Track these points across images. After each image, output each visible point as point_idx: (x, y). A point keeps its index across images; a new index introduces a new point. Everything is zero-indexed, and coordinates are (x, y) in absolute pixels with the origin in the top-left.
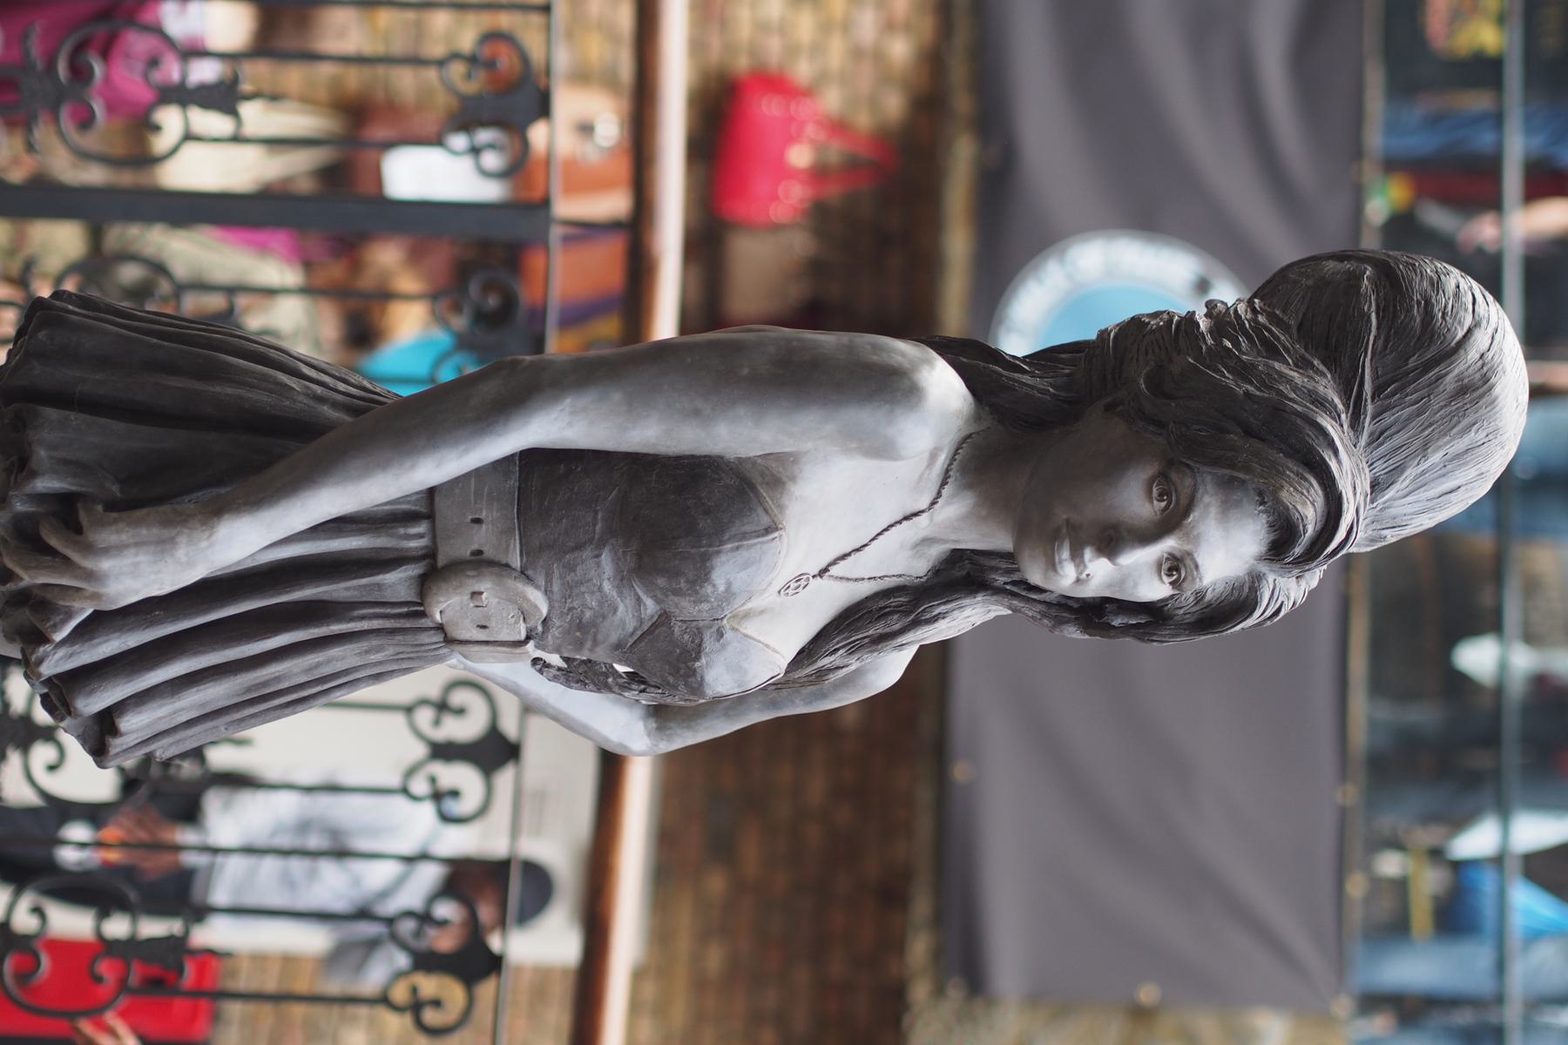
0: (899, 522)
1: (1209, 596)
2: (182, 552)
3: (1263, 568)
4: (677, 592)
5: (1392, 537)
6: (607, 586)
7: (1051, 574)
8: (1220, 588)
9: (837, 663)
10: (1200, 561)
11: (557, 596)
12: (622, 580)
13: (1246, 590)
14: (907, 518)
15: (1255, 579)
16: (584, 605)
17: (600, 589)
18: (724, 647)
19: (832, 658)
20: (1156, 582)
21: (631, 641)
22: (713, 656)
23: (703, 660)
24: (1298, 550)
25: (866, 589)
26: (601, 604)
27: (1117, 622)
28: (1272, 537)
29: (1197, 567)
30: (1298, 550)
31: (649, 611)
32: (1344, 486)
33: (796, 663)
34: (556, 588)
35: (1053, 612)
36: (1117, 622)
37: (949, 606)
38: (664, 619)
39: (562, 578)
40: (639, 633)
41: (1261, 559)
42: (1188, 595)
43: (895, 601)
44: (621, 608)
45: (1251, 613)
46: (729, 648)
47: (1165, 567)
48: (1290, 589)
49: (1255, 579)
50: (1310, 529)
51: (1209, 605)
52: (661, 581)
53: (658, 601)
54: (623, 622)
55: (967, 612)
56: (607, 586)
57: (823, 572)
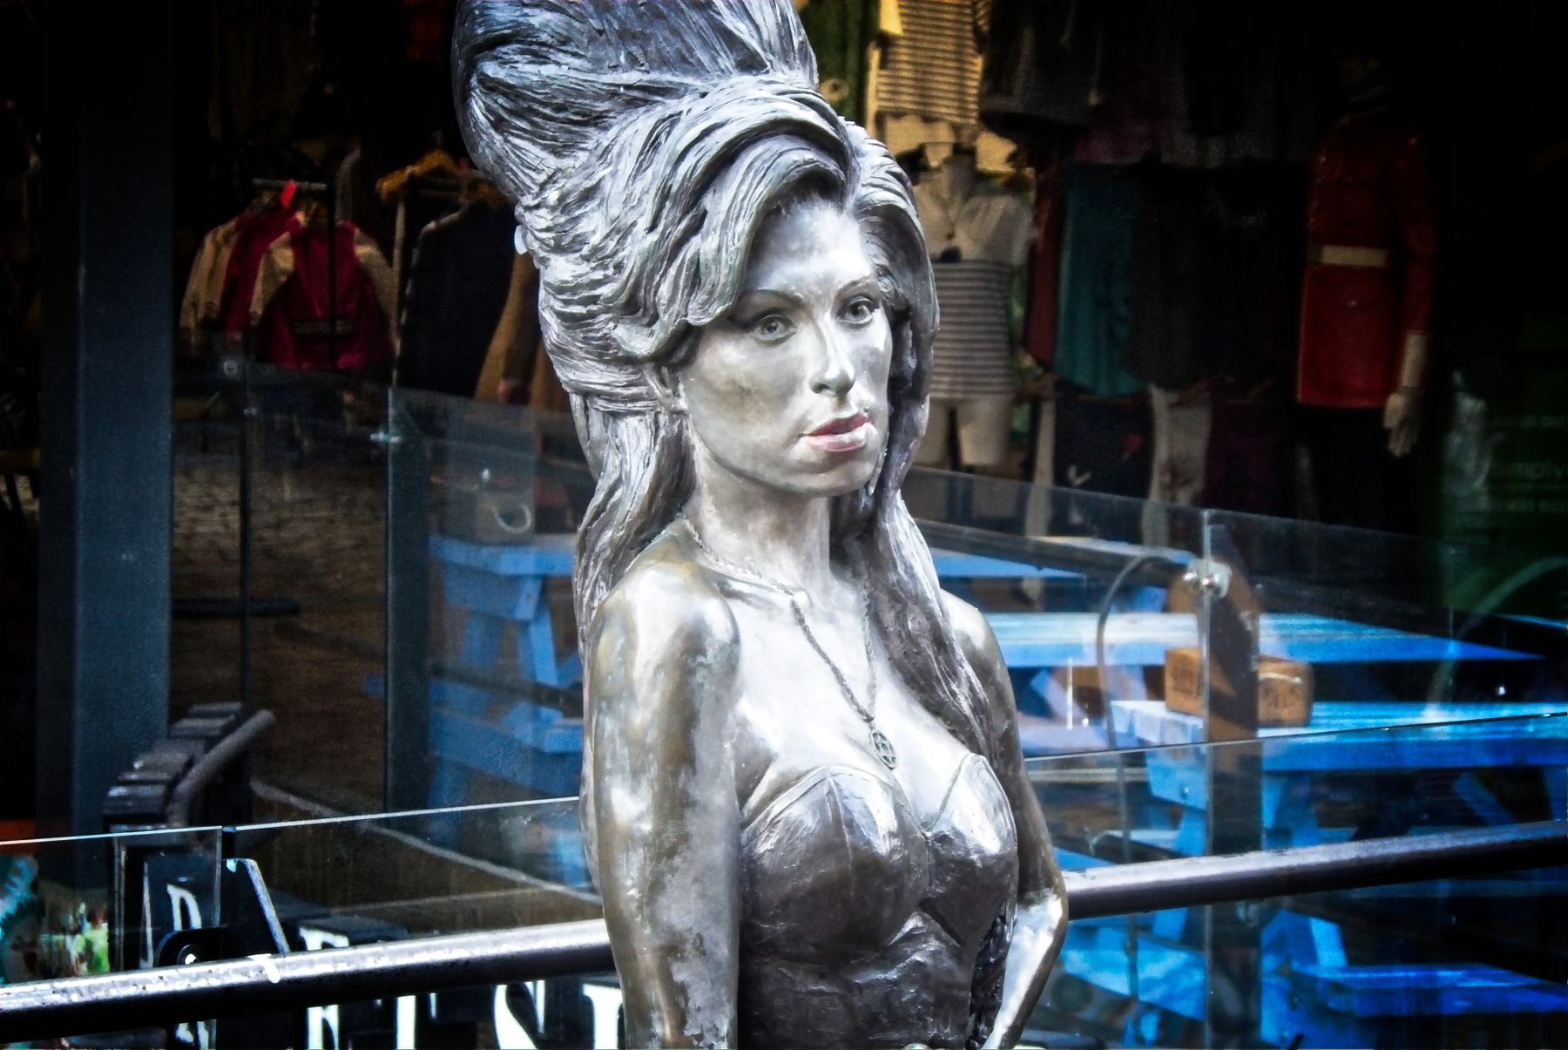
0: (805, 629)
1: (884, 261)
2: (1090, 872)
3: (850, 202)
4: (898, 893)
5: (798, 37)
6: (893, 975)
7: (866, 452)
8: (874, 249)
9: (965, 690)
10: (847, 281)
11: (904, 1034)
12: (888, 957)
13: (875, 219)
14: (801, 621)
15: (865, 210)
16: (913, 1001)
17: (895, 983)
18: (958, 834)
19: (961, 698)
20: (871, 330)
21: (954, 942)
22: (970, 845)
23: (974, 857)
24: (832, 166)
25: (882, 668)
26: (913, 983)
27: (912, 363)
28: (816, 196)
29: (854, 283)
30: (832, 166)
31: (920, 924)
32: (756, 116)
33: (972, 744)
34: (896, 1036)
35: (901, 437)
36: (912, 363)
37: (898, 563)
38: (927, 906)
39: (884, 1030)
40: (944, 934)
41: (841, 208)
42: (884, 286)
43: (889, 617)
44: (917, 957)
45: (903, 211)
46: (961, 828)
47: (852, 319)
48: (873, 164)
49: (865, 210)
50: (809, 155)
51: (891, 258)
52: (887, 913)
53: (907, 916)
54: (934, 954)
55: (902, 538)
56: (893, 975)
57: (869, 720)
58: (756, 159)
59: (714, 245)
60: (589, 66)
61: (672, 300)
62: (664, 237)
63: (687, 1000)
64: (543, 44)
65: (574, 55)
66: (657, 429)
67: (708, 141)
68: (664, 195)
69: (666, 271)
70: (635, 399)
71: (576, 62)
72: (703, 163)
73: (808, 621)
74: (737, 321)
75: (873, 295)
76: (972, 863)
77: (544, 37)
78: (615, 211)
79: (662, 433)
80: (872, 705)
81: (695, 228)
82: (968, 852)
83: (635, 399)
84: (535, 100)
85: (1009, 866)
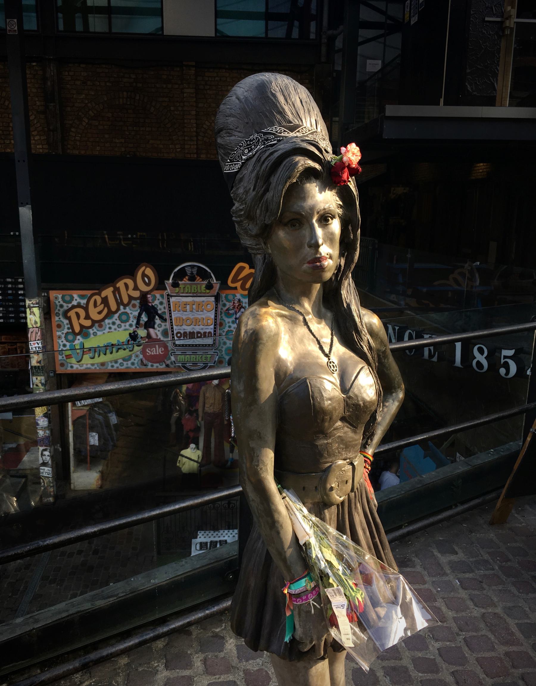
9: (366, 344)
23: (361, 403)
38: (343, 419)
58: (287, 163)
59: (272, 195)
60: (243, 135)
61: (260, 215)
62: (258, 193)
63: (254, 453)
64: (230, 129)
65: (239, 132)
66: (265, 259)
67: (272, 157)
68: (257, 177)
69: (259, 205)
70: (258, 249)
71: (240, 134)
72: (269, 165)
73: (310, 324)
74: (282, 222)
75: (333, 214)
76: (360, 405)
77: (231, 127)
78: (245, 185)
79: (266, 261)
80: (330, 351)
81: (267, 190)
82: (358, 401)
83: (258, 249)
84: (229, 149)
85: (373, 404)
